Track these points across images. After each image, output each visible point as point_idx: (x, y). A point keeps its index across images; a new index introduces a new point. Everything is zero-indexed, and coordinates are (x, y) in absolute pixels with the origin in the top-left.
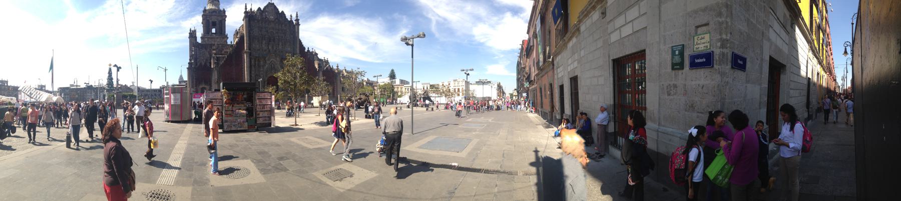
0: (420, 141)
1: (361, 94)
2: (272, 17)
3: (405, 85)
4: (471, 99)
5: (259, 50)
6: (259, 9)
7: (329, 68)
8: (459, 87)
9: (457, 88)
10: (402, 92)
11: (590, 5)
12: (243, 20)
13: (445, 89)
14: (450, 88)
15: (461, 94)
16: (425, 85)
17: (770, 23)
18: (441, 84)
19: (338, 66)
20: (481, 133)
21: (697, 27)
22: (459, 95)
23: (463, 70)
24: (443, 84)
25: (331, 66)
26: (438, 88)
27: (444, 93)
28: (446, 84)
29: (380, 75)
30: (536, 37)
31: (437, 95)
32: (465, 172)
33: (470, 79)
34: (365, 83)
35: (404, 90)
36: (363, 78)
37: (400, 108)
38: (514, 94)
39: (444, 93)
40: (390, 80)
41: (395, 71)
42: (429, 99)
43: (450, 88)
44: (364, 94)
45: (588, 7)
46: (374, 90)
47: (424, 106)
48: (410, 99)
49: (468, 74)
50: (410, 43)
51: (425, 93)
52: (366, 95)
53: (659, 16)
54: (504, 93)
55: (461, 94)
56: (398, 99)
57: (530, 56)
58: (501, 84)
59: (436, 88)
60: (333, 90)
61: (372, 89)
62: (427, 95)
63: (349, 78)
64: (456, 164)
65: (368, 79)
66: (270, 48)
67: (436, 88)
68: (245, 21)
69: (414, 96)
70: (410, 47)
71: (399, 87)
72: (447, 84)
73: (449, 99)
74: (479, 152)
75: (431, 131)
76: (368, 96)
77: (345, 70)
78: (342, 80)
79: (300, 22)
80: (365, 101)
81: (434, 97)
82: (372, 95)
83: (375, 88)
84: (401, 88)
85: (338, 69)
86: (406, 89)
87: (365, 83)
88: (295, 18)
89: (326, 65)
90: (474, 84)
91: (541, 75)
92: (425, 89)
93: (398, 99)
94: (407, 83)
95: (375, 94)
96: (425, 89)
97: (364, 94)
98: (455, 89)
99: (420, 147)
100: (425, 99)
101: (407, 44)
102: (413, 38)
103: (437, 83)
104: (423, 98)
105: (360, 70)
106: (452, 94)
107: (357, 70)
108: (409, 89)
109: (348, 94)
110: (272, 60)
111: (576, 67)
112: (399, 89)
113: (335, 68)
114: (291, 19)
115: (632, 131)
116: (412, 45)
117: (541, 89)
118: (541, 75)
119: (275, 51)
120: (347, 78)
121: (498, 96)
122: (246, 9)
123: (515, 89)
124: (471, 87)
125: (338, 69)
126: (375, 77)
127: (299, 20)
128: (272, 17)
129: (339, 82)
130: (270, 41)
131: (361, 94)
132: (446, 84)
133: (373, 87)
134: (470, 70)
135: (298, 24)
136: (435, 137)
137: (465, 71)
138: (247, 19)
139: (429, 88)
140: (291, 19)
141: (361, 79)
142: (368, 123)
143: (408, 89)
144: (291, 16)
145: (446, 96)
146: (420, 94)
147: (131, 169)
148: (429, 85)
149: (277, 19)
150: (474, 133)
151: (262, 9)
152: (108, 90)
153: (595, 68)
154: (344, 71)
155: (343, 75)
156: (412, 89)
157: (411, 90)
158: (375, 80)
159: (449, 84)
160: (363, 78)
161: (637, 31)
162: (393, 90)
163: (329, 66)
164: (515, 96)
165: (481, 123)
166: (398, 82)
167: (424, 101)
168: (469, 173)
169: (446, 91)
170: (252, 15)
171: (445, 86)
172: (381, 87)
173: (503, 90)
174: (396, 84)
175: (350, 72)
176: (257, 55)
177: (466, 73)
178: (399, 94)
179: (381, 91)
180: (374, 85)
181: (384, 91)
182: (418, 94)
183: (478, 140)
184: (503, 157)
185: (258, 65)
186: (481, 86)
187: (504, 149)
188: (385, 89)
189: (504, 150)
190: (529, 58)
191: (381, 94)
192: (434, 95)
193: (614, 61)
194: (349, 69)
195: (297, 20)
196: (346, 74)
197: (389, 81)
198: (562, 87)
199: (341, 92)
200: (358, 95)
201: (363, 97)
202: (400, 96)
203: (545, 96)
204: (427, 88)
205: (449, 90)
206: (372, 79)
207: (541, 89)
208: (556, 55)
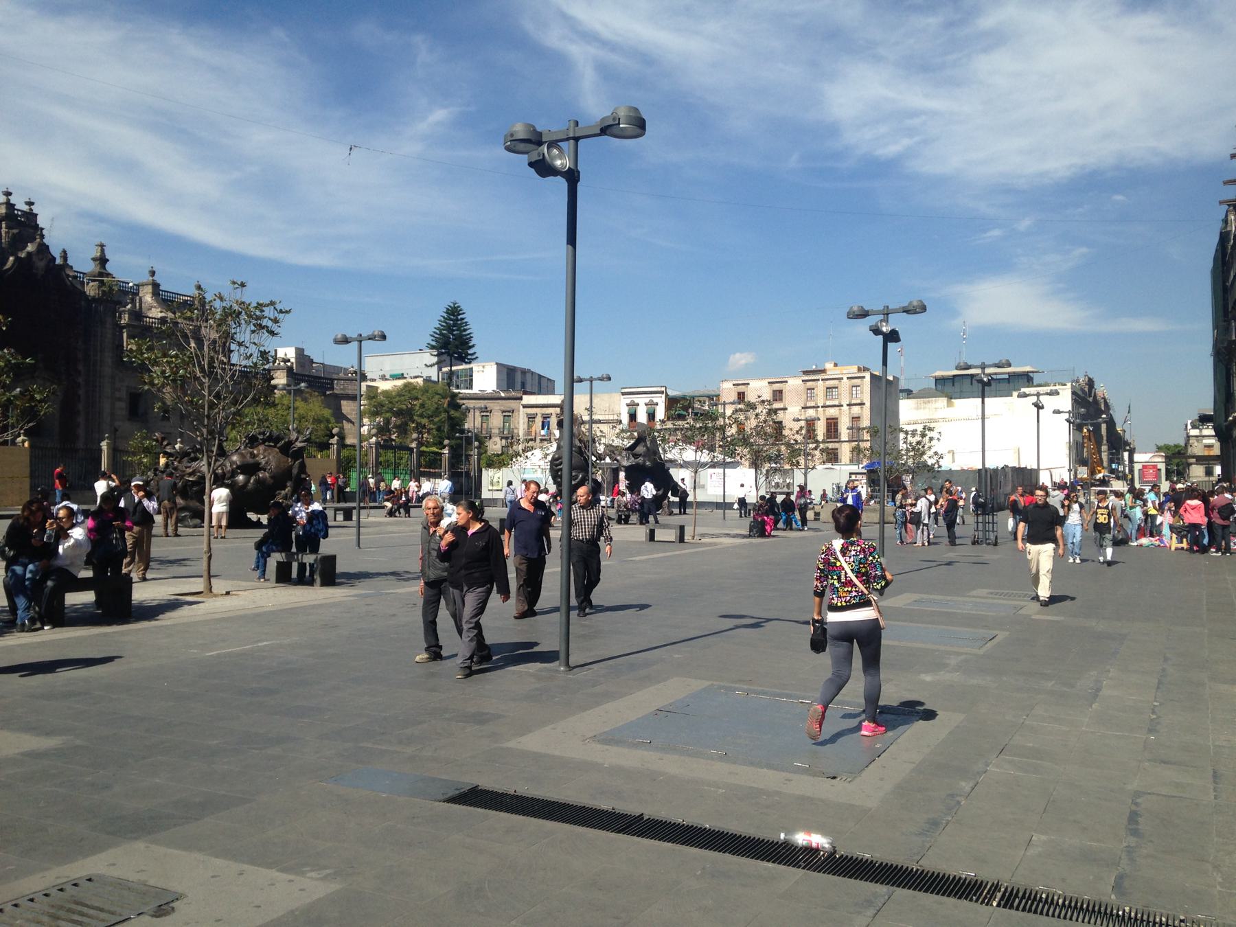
0: (610, 706)
1: (252, 441)
3: (527, 399)
4: (907, 479)
7: (41, 264)
8: (832, 412)
9: (822, 415)
10: (509, 438)
13: (752, 423)
14: (780, 416)
15: (845, 451)
16: (642, 400)
18: (728, 391)
19: (102, 261)
20: (974, 681)
22: (832, 457)
23: (864, 314)
24: (741, 396)
25: (56, 252)
26: (714, 418)
27: (745, 441)
28: (759, 389)
31: (705, 457)
32: (882, 889)
33: (902, 366)
34: (280, 379)
35: (520, 424)
36: (268, 343)
38: (1197, 449)
39: (745, 441)
40: (440, 364)
42: (660, 474)
43: (780, 416)
44: (273, 440)
46: (340, 417)
47: (634, 518)
48: (556, 474)
49: (893, 337)
50: (558, 163)
51: (640, 440)
52: (286, 449)
54: (1118, 444)
55: (845, 451)
56: (488, 475)
58: (1101, 389)
59: (698, 415)
60: (68, 408)
61: (327, 413)
62: (653, 452)
63: (169, 334)
64: (818, 840)
65: (300, 353)
67: (698, 415)
69: (577, 459)
70: (561, 184)
71: (496, 406)
72: (767, 395)
73: (777, 479)
74: (966, 786)
75: (677, 654)
76: (299, 454)
77: (156, 286)
78: (129, 345)
80: (280, 479)
81: (685, 465)
82: (325, 446)
83: (347, 407)
84: (508, 414)
86: (531, 418)
87: (280, 379)
89: (18, 242)
90: (924, 394)
92: (642, 418)
93: (488, 475)
94: (543, 385)
95: (342, 445)
96: (642, 418)
97: (273, 440)
98: (811, 424)
99: (608, 739)
100: (636, 477)
101: (543, 168)
102: (577, 139)
103: (710, 390)
104: (628, 470)
105: (251, 297)
106: (794, 453)
107: (233, 297)
108: (554, 421)
109: (169, 438)
112: (496, 421)
113: (82, 263)
115: (179, 440)
116: (572, 177)
120: (161, 335)
121: (1082, 462)
123: (1204, 419)
124: (909, 412)
125: (103, 273)
126: (346, 340)
129: (108, 358)
131: (252, 441)
132: (759, 389)
133: (334, 402)
134: (907, 311)
136: (697, 685)
137: (872, 320)
139: (660, 414)
141: (253, 349)
142: (293, 611)
143: (546, 417)
145: (755, 465)
146: (612, 450)
147: (92, 590)
148: (661, 401)
150: (928, 678)
155: (138, 315)
156: (568, 420)
157: (560, 424)
158: (343, 358)
159: (778, 395)
160: (268, 343)
162: (456, 425)
163: (44, 249)
164: (1200, 460)
165: (971, 621)
166: (485, 378)
167: (634, 487)
168: (901, 893)
169: (759, 431)
171: (752, 406)
172: (380, 404)
173: (1111, 423)
174: (476, 390)
175: (187, 305)
177: (876, 331)
178: (495, 446)
179: (382, 430)
180: (338, 388)
181: (403, 430)
182: (601, 449)
183: (961, 717)
184: (1135, 833)
186: (968, 406)
187: (1134, 785)
188: (406, 414)
189: (1138, 794)
191: (384, 446)
192: (689, 454)
194: (179, 283)
196: (156, 313)
197: (433, 373)
199: (125, 426)
200: (235, 441)
201: (268, 457)
202: (499, 461)
204: (651, 416)
205: (779, 426)
206: (328, 355)
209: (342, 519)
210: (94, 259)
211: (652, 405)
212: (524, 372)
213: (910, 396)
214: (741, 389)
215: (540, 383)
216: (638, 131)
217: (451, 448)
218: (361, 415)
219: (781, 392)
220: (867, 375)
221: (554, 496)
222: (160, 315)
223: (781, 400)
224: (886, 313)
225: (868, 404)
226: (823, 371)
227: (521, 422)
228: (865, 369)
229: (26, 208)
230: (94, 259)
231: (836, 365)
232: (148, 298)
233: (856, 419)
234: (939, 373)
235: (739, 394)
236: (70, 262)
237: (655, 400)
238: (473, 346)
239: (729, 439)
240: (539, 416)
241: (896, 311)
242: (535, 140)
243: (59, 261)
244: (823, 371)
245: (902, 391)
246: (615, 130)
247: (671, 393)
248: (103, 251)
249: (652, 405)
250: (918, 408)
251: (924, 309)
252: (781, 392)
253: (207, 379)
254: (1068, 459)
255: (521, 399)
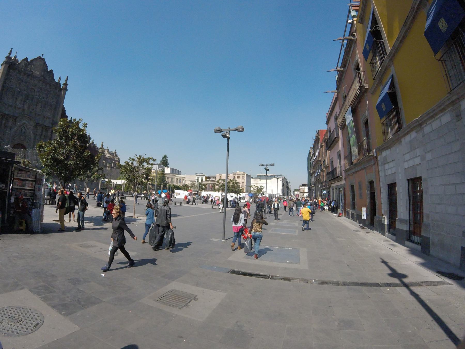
2: (38, 73)
3: (177, 175)
5: (11, 106)
6: (26, 59)
7: (92, 146)
11: (437, 108)
12: (2, 65)
17: (84, 135)
19: (103, 145)
21: (404, 155)
23: (263, 165)
25: (95, 144)
29: (239, 126)
30: (12, 172)
37: (179, 204)
41: (168, 159)
45: (435, 110)
53: (351, 87)
57: (332, 148)
66: (26, 107)
68: (3, 66)
77: (108, 150)
79: (68, 87)
84: (172, 179)
85: (102, 148)
86: (177, 179)
88: (64, 82)
90: (255, 178)
91: (353, 170)
92: (200, 181)
96: (200, 181)
102: (230, 131)
110: (24, 122)
111: (419, 164)
114: (59, 81)
117: (352, 187)
118: (353, 170)
119: (31, 112)
122: (10, 54)
127: (68, 85)
128: (38, 73)
130: (27, 99)
135: (66, 89)
138: (7, 66)
139: (204, 180)
140: (59, 81)
143: (180, 179)
144: (60, 78)
149: (43, 76)
151: (29, 61)
152: (80, 151)
153: (449, 175)
154: (106, 152)
161: (334, 92)
170: (15, 64)
175: (113, 154)
176: (7, 113)
177: (266, 169)
185: (5, 126)
190: (330, 150)
193: (388, 185)
195: (66, 84)
196: (108, 155)
198: (392, 187)
203: (361, 195)
204: (202, 180)
207: (352, 187)
208: (380, 150)
209: (78, 206)
210: (101, 145)
211: (202, 178)
212: (175, 170)
213: (410, 182)
214: (220, 176)
215: (178, 172)
216: (243, 130)
217: (163, 185)
218: (255, 192)
219: (239, 177)
220: (245, 174)
221: (5, 187)
222: (108, 155)
223: (239, 178)
224: (267, 165)
225: (245, 180)
226: (237, 173)
227: (175, 180)
228: (245, 173)
229: (88, 135)
230: (101, 145)
231: (239, 172)
232: (106, 152)
233: (243, 183)
234: (258, 174)
235: (220, 177)
236: (97, 145)
237: (203, 177)
238: (169, 165)
239: (143, 195)
240: (182, 179)
241: (269, 165)
242: (221, 131)
243: (95, 145)
244: (237, 173)
245: (252, 178)
246: (238, 130)
247: (206, 176)
248: (103, 143)
249: (202, 178)
250: (254, 181)
251: (274, 165)
252: (239, 177)
253: (153, 174)
254: (408, 212)
255: (175, 175)
